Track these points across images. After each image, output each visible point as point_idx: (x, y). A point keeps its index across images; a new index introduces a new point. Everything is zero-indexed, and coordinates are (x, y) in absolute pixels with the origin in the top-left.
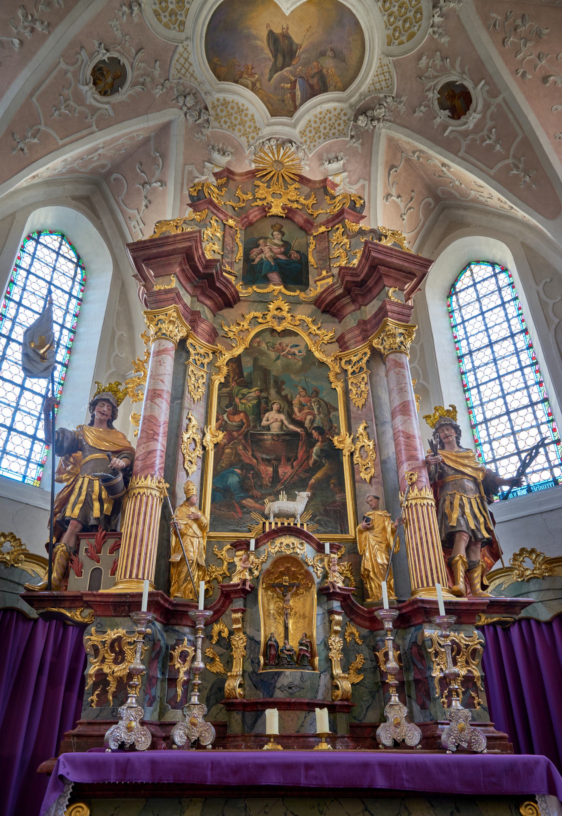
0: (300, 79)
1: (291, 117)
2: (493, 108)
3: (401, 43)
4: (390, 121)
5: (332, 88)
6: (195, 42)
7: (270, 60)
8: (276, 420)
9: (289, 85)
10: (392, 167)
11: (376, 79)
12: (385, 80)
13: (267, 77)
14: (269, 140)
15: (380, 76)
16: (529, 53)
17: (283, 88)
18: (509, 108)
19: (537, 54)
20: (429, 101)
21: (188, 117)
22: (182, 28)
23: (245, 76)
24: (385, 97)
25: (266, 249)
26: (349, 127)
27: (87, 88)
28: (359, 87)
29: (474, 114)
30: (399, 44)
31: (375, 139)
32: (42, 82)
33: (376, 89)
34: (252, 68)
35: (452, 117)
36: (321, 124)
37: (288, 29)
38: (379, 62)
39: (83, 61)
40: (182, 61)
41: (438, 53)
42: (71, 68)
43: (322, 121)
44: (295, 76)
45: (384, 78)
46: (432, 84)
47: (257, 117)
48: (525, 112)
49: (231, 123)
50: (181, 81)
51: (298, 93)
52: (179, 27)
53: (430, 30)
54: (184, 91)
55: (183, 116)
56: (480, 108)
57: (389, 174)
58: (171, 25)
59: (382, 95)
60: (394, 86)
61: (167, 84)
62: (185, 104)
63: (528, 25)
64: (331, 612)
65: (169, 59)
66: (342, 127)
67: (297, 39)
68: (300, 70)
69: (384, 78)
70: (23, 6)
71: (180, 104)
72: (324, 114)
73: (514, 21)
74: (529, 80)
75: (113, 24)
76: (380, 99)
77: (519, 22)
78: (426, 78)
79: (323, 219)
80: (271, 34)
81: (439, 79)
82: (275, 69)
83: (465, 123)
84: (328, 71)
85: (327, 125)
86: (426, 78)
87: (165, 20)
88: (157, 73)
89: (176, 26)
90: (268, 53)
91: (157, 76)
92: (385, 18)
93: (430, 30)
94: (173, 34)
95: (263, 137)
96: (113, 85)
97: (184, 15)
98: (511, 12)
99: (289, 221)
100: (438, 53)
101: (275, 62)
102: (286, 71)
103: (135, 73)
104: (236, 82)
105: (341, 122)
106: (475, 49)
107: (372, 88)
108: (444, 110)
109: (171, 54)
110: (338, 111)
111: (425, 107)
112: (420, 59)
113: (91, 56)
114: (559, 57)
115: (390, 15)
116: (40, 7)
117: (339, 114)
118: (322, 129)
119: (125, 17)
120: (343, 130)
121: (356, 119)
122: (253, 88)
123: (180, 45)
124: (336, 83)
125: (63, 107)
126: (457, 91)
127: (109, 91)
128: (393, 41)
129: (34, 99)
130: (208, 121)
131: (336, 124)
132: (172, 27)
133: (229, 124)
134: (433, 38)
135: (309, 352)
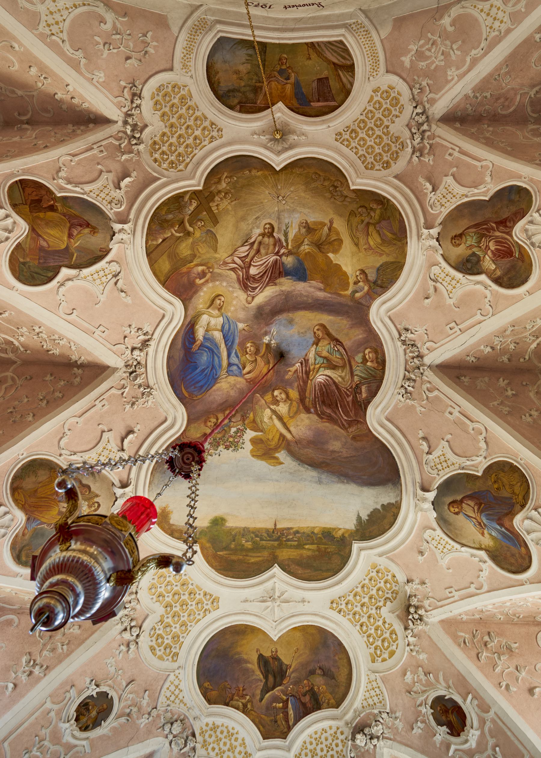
0: (292, 698)
1: (285, 738)
2: (488, 724)
3: (384, 660)
4: (390, 739)
5: (325, 705)
6: (187, 670)
7: (261, 681)
9: (281, 705)
11: (367, 694)
12: (377, 695)
13: (258, 697)
15: (371, 692)
16: (507, 667)
17: (275, 708)
18: (504, 723)
19: (514, 666)
20: (424, 717)
21: (173, 746)
22: (175, 658)
23: (236, 698)
24: (380, 712)
26: (347, 747)
27: (67, 725)
28: (351, 704)
29: (471, 731)
30: (382, 661)
32: (21, 725)
33: (369, 705)
34: (243, 690)
35: (452, 734)
36: (317, 745)
37: (277, 652)
38: (367, 678)
39: (70, 698)
40: (172, 688)
41: (420, 669)
42: (56, 707)
43: (318, 741)
44: (286, 695)
45: (375, 694)
46: (423, 698)
47: (248, 741)
48: (522, 728)
49: (220, 749)
50: (169, 708)
51: (291, 712)
52: (172, 657)
53: (408, 648)
54: (171, 718)
55: (167, 744)
56: (476, 724)
58: (164, 656)
59: (376, 711)
60: (386, 701)
61: (154, 713)
62: (171, 732)
63: (496, 641)
65: (159, 688)
66: (340, 747)
67: (286, 661)
68: (291, 689)
69: (375, 694)
70: (29, 653)
71: (166, 732)
72: (319, 734)
73: (482, 638)
74: (515, 692)
75: (109, 661)
76: (375, 715)
77: (486, 638)
78: (415, 692)
80: (261, 657)
81: (428, 694)
82: (266, 690)
83: (466, 741)
84: (319, 688)
85: (323, 746)
86: (415, 692)
87: (159, 653)
88: (145, 703)
89: (170, 658)
90: (259, 675)
91: (145, 705)
92: (365, 639)
93: (408, 648)
94: (167, 664)
96: (96, 718)
97: (178, 648)
98: (476, 631)
100: (420, 669)
101: (266, 683)
102: (278, 691)
103: (122, 705)
104: (227, 704)
105: (339, 741)
106: (453, 665)
107: (365, 704)
108: (442, 726)
109: (162, 682)
110: (334, 729)
111: (422, 723)
112: (405, 675)
113: (80, 693)
114: (537, 669)
115: (369, 636)
116: (45, 653)
117: (336, 733)
118: (318, 751)
119: (121, 655)
120: (342, 751)
121: (353, 739)
122: (244, 710)
123: (172, 674)
124: (329, 700)
125: (35, 749)
126: (449, 706)
127: (91, 725)
128: (377, 658)
129: (6, 744)
130: (194, 749)
131: (334, 744)
132: (166, 658)
133: (217, 751)
134: (412, 656)
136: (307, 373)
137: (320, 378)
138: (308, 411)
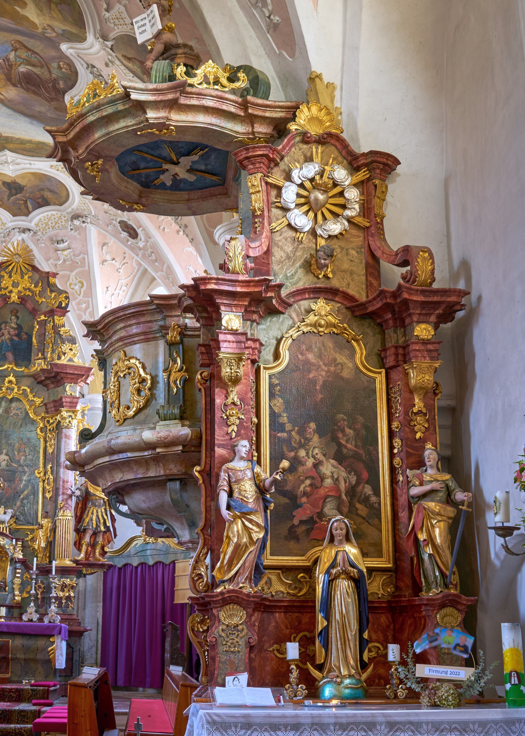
8: (4, 460)
10: (104, 244)
14: (14, 229)
25: (6, 332)
31: (87, 232)
57: (102, 249)
64: (16, 569)
74: (168, 232)
79: (44, 309)
95: (8, 228)
99: (22, 306)
135: (27, 413)
136: (11, 66)
137: (22, 69)
138: (15, 85)
